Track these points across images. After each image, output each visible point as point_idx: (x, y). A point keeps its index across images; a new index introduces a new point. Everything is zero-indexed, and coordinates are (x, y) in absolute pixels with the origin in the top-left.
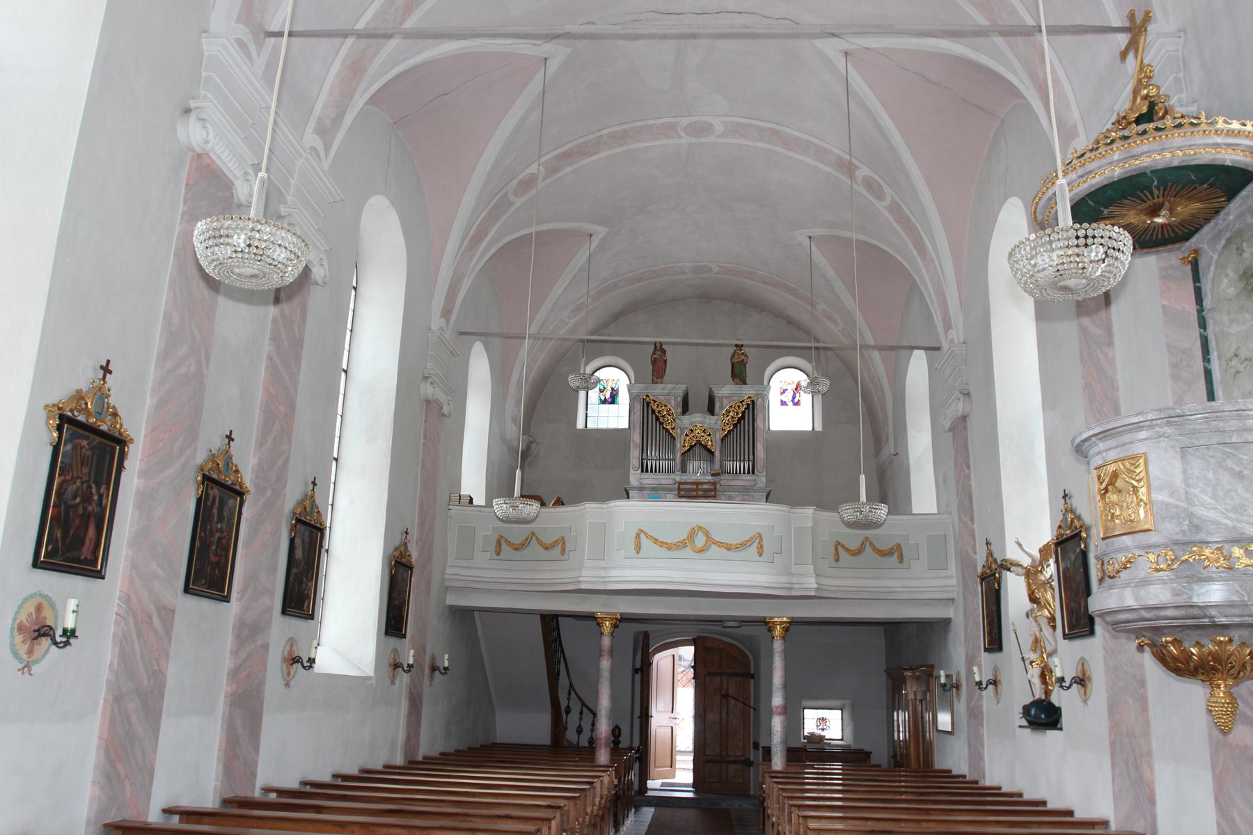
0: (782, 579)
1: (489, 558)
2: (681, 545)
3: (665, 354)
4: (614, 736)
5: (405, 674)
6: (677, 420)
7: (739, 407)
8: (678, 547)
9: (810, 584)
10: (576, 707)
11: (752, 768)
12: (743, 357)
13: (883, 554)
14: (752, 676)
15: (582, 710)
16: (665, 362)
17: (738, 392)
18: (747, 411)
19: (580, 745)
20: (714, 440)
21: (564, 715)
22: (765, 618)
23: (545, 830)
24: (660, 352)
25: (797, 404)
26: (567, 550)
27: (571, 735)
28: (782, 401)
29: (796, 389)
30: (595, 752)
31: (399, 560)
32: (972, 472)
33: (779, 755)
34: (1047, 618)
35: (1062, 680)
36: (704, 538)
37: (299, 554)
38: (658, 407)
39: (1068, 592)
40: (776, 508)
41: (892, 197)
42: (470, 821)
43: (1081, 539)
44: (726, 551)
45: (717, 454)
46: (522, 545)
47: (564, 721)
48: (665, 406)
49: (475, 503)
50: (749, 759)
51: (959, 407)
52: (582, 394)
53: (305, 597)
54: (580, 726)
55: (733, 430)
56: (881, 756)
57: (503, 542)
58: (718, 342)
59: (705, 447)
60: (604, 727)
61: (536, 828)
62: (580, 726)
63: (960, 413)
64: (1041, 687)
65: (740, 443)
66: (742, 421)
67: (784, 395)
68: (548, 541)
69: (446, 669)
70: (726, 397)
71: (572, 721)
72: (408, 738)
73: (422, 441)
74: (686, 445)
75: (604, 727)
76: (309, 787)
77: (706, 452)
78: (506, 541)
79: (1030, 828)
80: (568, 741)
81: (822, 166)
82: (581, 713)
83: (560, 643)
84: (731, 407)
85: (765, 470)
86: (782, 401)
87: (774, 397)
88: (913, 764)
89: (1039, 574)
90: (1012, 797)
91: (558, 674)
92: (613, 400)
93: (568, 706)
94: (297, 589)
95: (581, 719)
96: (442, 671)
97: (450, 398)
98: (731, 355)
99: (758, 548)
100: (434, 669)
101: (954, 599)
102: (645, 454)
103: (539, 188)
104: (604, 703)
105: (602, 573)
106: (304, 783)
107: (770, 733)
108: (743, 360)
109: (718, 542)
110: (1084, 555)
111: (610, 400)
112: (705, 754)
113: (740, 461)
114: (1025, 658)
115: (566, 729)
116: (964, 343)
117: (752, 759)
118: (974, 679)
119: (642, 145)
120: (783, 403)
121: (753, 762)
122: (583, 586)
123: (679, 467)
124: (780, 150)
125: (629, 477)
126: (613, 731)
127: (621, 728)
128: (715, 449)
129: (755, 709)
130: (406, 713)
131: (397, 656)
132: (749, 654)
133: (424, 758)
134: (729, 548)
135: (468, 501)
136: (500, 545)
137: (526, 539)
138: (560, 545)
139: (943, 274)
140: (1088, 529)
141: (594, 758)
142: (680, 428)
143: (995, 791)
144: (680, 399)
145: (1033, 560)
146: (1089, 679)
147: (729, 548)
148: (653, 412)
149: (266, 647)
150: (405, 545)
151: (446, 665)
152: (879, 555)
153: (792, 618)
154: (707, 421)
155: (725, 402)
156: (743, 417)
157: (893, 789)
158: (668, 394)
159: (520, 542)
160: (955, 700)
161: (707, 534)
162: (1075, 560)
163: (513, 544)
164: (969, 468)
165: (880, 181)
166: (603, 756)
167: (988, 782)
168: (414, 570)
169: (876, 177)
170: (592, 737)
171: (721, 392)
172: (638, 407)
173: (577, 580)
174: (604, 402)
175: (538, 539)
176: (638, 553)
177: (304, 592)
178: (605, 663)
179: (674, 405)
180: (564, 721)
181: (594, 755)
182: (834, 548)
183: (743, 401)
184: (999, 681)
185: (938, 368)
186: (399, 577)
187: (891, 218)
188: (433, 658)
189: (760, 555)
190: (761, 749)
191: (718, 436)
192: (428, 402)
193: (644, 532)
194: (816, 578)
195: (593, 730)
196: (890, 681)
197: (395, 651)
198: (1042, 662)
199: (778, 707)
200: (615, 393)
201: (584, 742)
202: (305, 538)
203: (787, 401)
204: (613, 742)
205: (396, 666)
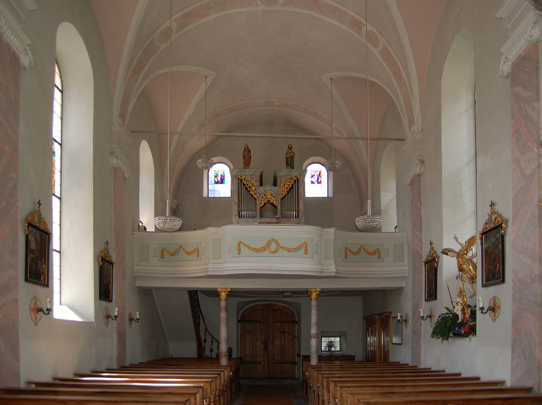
0: (318, 267)
1: (157, 260)
2: (263, 249)
3: (250, 152)
4: (229, 353)
5: (114, 321)
6: (257, 189)
7: (290, 181)
8: (262, 250)
9: (331, 269)
10: (209, 339)
11: (296, 366)
12: (292, 154)
13: (370, 254)
14: (297, 322)
15: (212, 340)
16: (250, 157)
17: (290, 173)
18: (294, 184)
19: (212, 357)
20: (277, 200)
21: (203, 343)
22: (307, 289)
23: (193, 400)
24: (247, 151)
25: (320, 183)
26: (200, 254)
27: (207, 353)
28: (312, 181)
29: (319, 175)
30: (220, 360)
31: (104, 258)
32: (422, 206)
33: (314, 358)
34: (469, 278)
35: (482, 308)
36: (276, 245)
37: (33, 246)
38: (246, 182)
39: (488, 261)
40: (316, 228)
41: (384, 44)
42: (147, 397)
43: (502, 228)
44: (287, 252)
45: (279, 207)
46: (175, 252)
47: (204, 346)
48: (251, 181)
49: (147, 230)
50: (295, 361)
51: (417, 170)
52: (205, 172)
53: (41, 273)
54: (211, 348)
55: (287, 194)
56: (359, 356)
57: (164, 251)
58: (281, 136)
59: (272, 204)
60: (223, 347)
61: (186, 399)
62: (211, 348)
63: (417, 173)
64: (462, 316)
65: (291, 202)
66: (292, 189)
67: (313, 178)
68: (190, 250)
69: (138, 319)
70: (284, 176)
71: (208, 346)
72: (119, 355)
73: (113, 192)
74: (262, 202)
75: (223, 347)
76: (58, 380)
77: (272, 207)
78: (166, 251)
79: (463, 387)
80: (206, 355)
81: (342, 26)
82: (212, 342)
83: (200, 308)
84: (286, 182)
85: (304, 216)
86: (312, 181)
87: (308, 179)
88: (378, 360)
89: (465, 255)
90: (440, 372)
91: (199, 323)
92: (222, 181)
93: (205, 339)
94: (34, 267)
95: (212, 345)
96: (136, 321)
97: (128, 168)
98: (286, 153)
99: (305, 250)
100: (131, 320)
101: (406, 277)
102: (240, 208)
103: (172, 40)
104: (223, 334)
105: (220, 266)
106: (56, 379)
107: (309, 347)
108: (292, 156)
109: (283, 247)
110: (503, 237)
111: (220, 182)
112: (273, 360)
113: (291, 211)
114: (453, 301)
115: (205, 350)
116: (422, 132)
117: (296, 362)
118: (421, 315)
119: (235, 11)
120: (312, 182)
121: (297, 363)
122: (210, 273)
123: (258, 215)
124: (317, 15)
125: (232, 220)
126: (228, 350)
127: (232, 348)
128: (278, 205)
129: (298, 338)
130: (117, 342)
131: (108, 312)
132: (295, 312)
133: (130, 365)
134: (289, 250)
135: (144, 229)
136: (163, 253)
137: (177, 250)
138: (196, 252)
139: (412, 93)
140: (507, 221)
141: (220, 363)
142: (259, 194)
143: (428, 371)
144: (258, 178)
145: (462, 247)
146: (499, 307)
147: (289, 250)
148: (244, 185)
149: (16, 301)
150: (107, 249)
151: (138, 317)
152: (368, 254)
153: (322, 289)
154: (273, 190)
155: (283, 179)
156: (292, 187)
157: (369, 371)
158: (252, 175)
159: (174, 251)
160: (404, 328)
161: (277, 243)
162: (495, 242)
163: (170, 252)
164: (421, 204)
165: (377, 33)
166: (224, 361)
167: (422, 366)
168: (114, 265)
169: (375, 31)
170: (218, 353)
171: (281, 173)
172: (236, 182)
173: (206, 270)
174: (217, 183)
175: (184, 249)
176: (239, 254)
177: (40, 270)
178: (223, 315)
179: (255, 181)
180: (204, 346)
181: (219, 361)
182: (344, 251)
183: (292, 178)
184: (433, 315)
185: (404, 149)
186: (105, 268)
187: (381, 59)
188: (130, 314)
189: (306, 254)
190: (301, 356)
191: (279, 198)
192: (115, 169)
193: (242, 242)
194: (335, 266)
195: (218, 350)
196: (365, 322)
197: (107, 309)
198: (463, 302)
199: (314, 334)
200: (223, 177)
201: (214, 355)
202: (37, 237)
203: (314, 181)
204: (229, 355)
205: (108, 317)
